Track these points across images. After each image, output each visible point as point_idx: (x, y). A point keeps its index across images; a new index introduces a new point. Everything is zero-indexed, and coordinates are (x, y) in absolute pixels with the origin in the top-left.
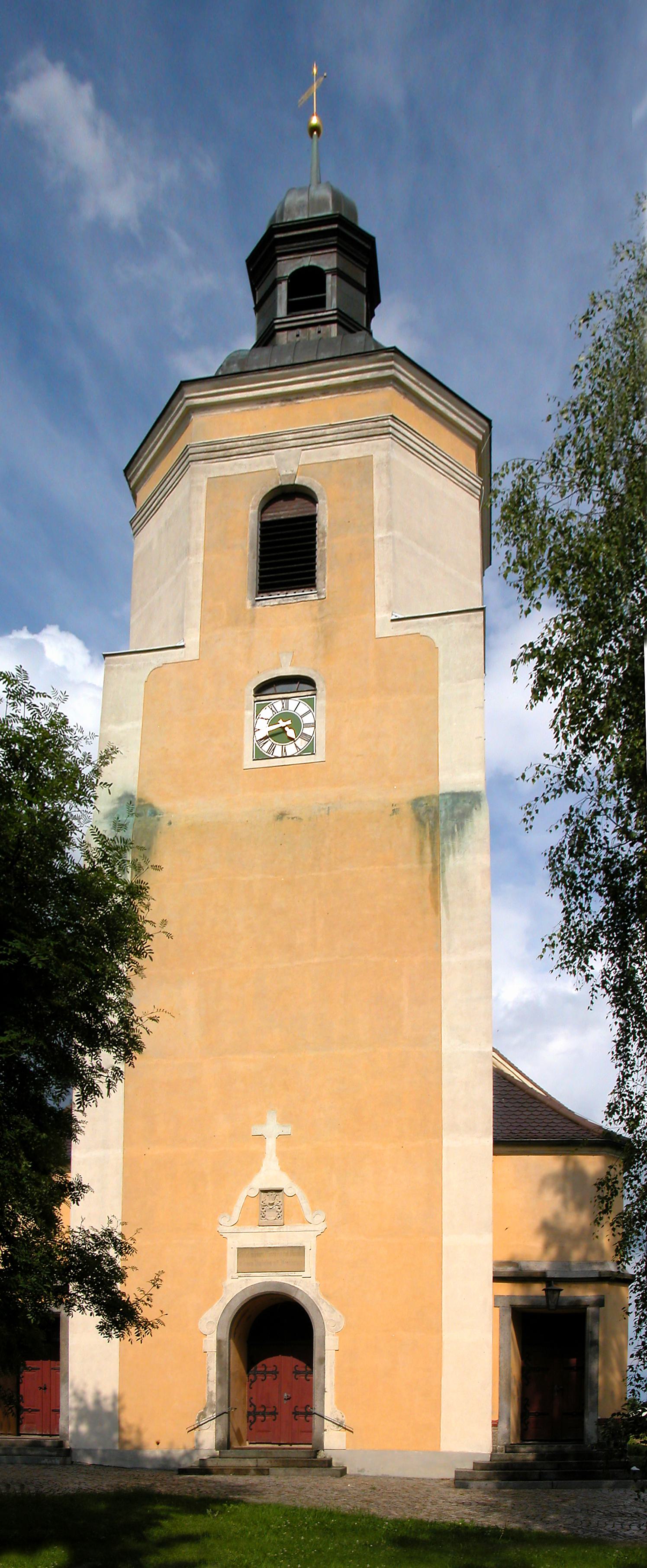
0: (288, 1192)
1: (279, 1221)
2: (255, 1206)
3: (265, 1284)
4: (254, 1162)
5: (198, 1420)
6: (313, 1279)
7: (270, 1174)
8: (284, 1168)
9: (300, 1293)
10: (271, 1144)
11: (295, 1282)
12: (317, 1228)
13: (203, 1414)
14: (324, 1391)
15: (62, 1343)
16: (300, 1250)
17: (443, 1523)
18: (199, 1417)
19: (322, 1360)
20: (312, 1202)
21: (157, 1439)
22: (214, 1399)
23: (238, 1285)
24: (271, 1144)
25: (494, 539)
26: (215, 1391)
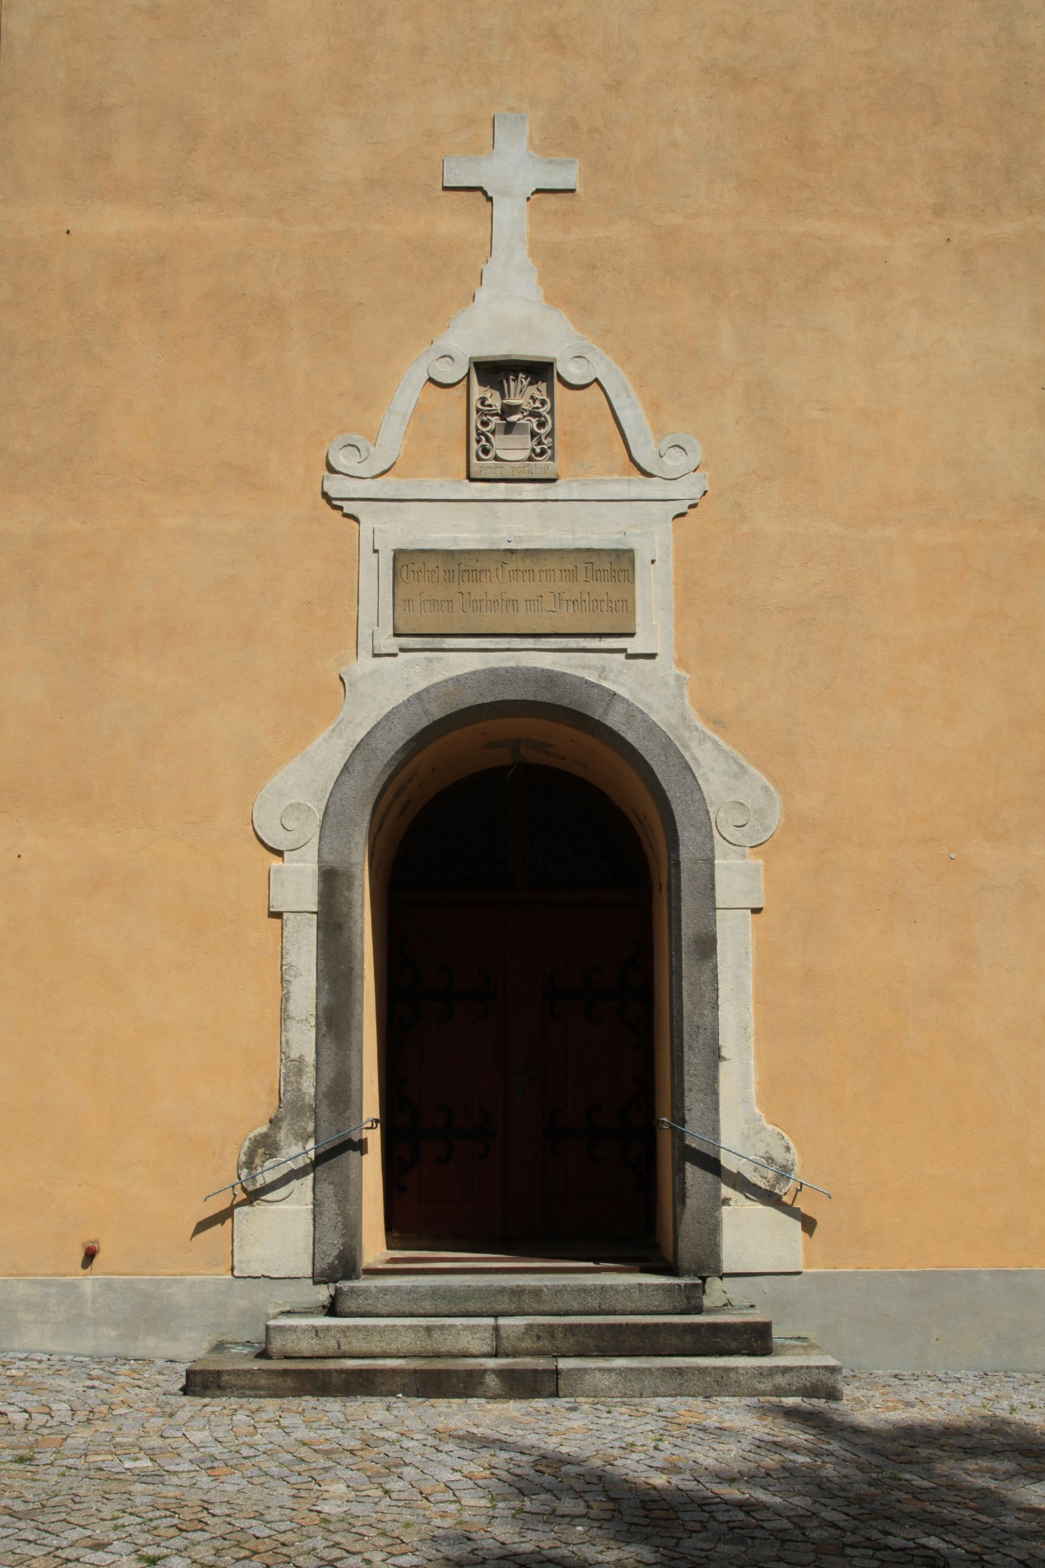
0: (570, 370)
1: (542, 467)
2: (451, 410)
3: (494, 675)
4: (454, 272)
5: (249, 1164)
6: (666, 666)
7: (509, 314)
8: (557, 297)
9: (620, 708)
10: (510, 215)
11: (602, 671)
12: (674, 490)
13: (265, 1145)
14: (716, 1056)
15: (354, 1024)
16: (619, 563)
17: (676, 584)
18: (251, 1154)
19: (707, 946)
20: (654, 407)
21: (88, 1236)
22: (308, 1085)
23: (392, 684)
24: (510, 215)
25: (973, 1512)
26: (310, 1057)
